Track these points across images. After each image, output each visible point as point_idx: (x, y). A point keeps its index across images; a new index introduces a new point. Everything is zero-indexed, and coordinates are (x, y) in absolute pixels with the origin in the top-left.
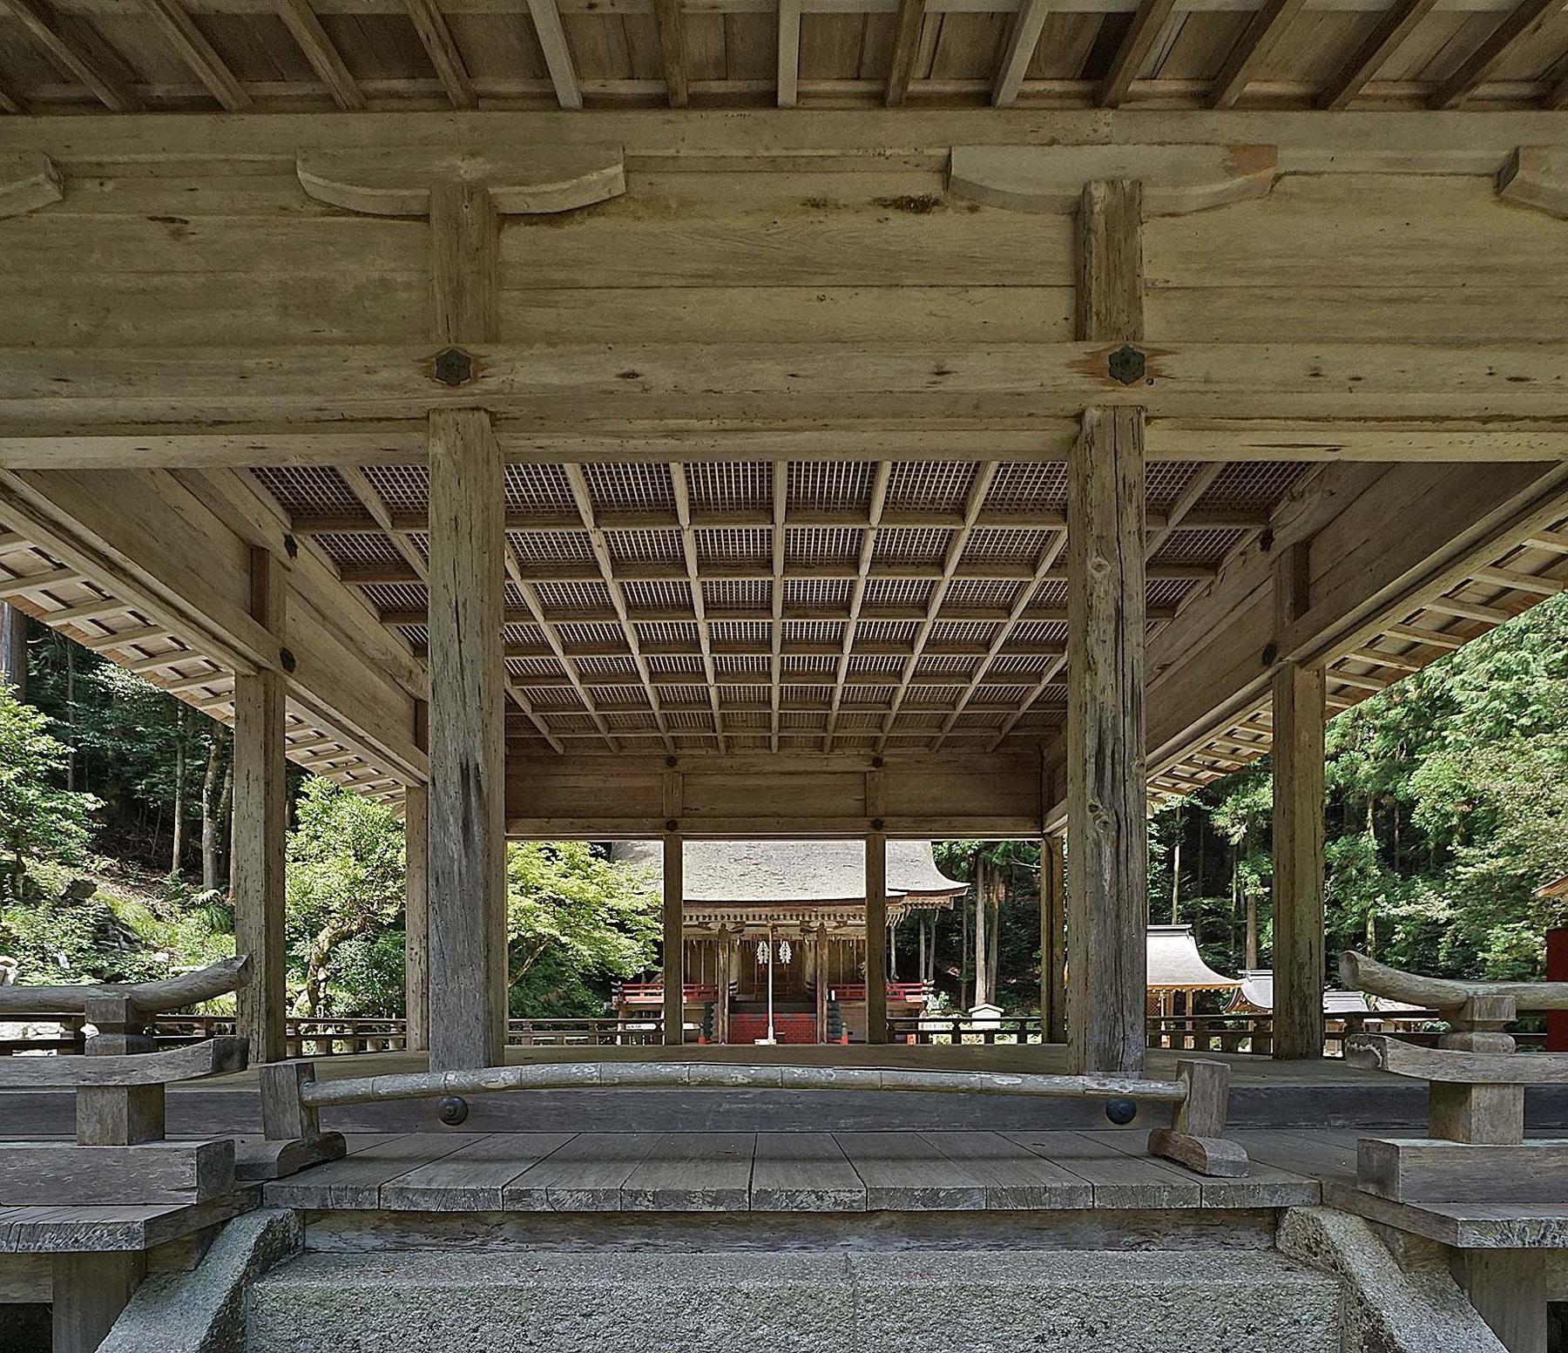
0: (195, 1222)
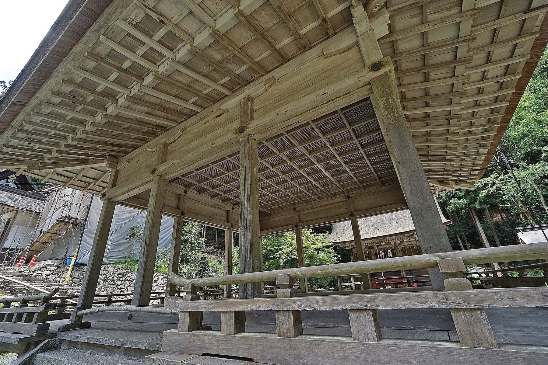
0: (34, 340)
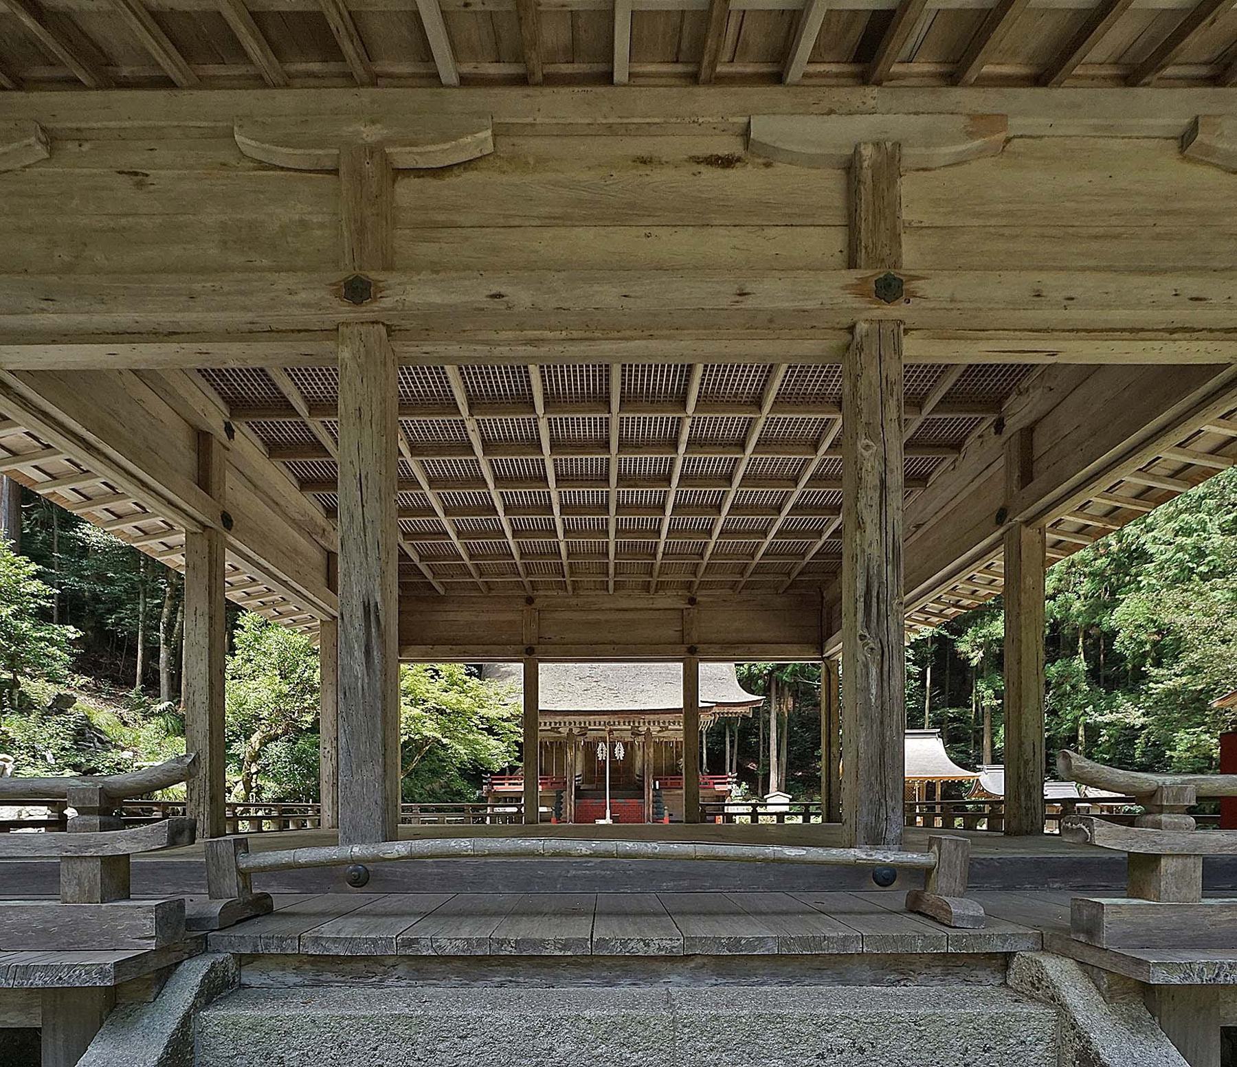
0: (154, 964)
